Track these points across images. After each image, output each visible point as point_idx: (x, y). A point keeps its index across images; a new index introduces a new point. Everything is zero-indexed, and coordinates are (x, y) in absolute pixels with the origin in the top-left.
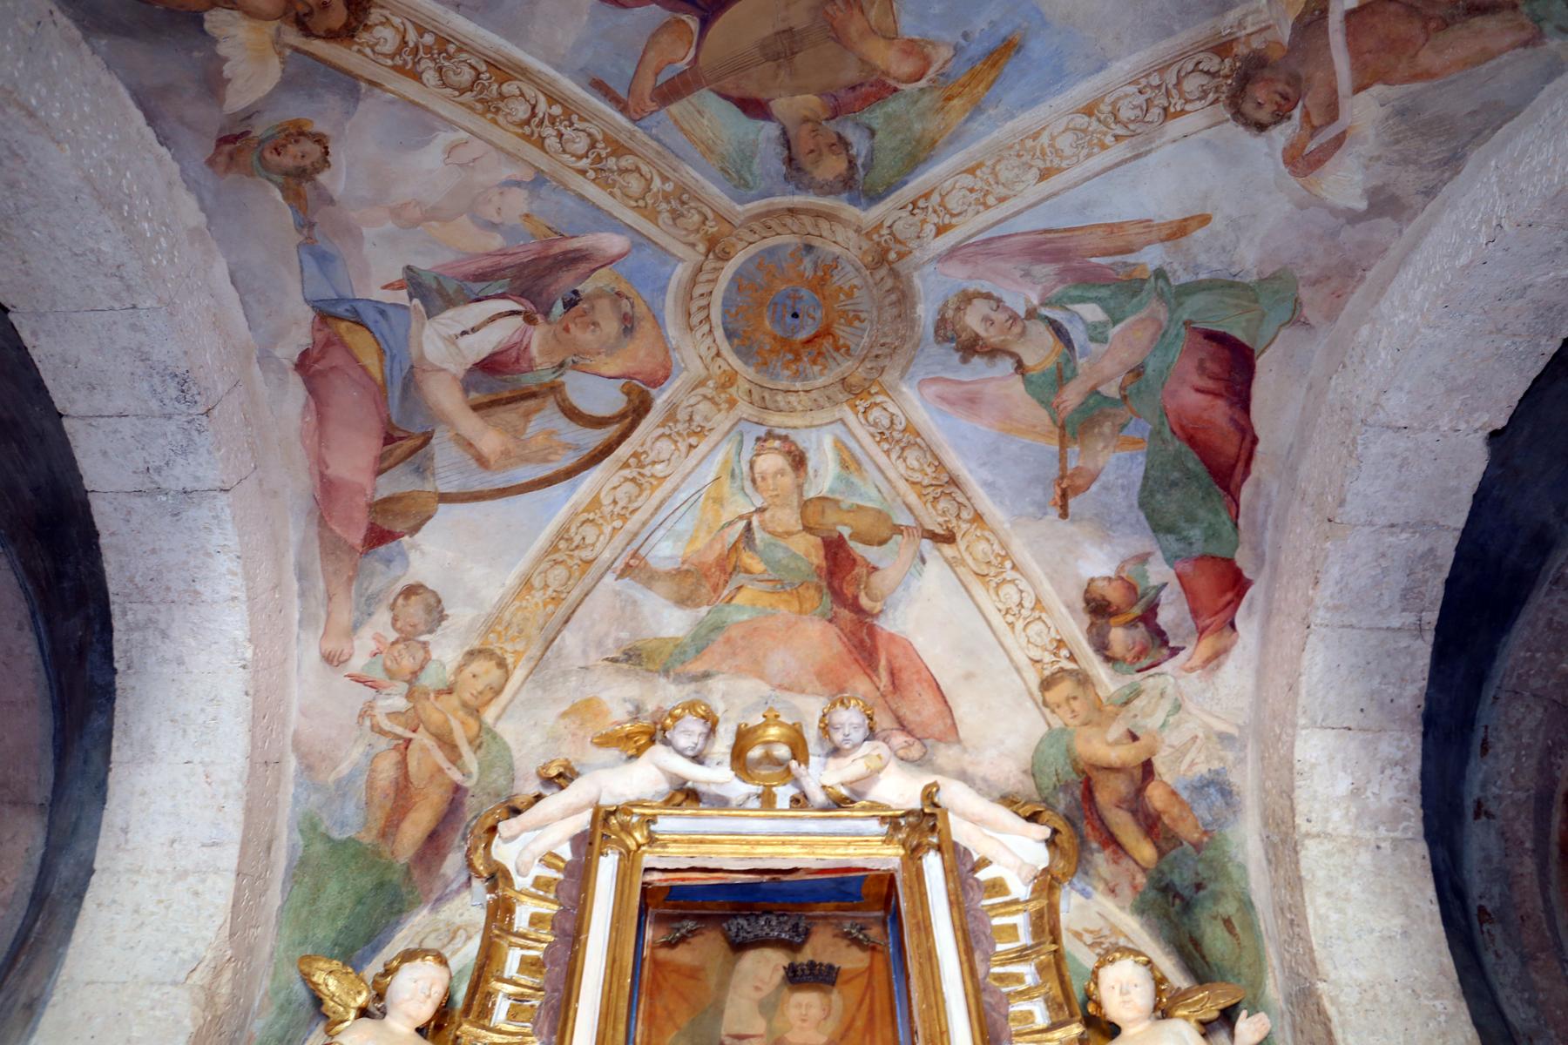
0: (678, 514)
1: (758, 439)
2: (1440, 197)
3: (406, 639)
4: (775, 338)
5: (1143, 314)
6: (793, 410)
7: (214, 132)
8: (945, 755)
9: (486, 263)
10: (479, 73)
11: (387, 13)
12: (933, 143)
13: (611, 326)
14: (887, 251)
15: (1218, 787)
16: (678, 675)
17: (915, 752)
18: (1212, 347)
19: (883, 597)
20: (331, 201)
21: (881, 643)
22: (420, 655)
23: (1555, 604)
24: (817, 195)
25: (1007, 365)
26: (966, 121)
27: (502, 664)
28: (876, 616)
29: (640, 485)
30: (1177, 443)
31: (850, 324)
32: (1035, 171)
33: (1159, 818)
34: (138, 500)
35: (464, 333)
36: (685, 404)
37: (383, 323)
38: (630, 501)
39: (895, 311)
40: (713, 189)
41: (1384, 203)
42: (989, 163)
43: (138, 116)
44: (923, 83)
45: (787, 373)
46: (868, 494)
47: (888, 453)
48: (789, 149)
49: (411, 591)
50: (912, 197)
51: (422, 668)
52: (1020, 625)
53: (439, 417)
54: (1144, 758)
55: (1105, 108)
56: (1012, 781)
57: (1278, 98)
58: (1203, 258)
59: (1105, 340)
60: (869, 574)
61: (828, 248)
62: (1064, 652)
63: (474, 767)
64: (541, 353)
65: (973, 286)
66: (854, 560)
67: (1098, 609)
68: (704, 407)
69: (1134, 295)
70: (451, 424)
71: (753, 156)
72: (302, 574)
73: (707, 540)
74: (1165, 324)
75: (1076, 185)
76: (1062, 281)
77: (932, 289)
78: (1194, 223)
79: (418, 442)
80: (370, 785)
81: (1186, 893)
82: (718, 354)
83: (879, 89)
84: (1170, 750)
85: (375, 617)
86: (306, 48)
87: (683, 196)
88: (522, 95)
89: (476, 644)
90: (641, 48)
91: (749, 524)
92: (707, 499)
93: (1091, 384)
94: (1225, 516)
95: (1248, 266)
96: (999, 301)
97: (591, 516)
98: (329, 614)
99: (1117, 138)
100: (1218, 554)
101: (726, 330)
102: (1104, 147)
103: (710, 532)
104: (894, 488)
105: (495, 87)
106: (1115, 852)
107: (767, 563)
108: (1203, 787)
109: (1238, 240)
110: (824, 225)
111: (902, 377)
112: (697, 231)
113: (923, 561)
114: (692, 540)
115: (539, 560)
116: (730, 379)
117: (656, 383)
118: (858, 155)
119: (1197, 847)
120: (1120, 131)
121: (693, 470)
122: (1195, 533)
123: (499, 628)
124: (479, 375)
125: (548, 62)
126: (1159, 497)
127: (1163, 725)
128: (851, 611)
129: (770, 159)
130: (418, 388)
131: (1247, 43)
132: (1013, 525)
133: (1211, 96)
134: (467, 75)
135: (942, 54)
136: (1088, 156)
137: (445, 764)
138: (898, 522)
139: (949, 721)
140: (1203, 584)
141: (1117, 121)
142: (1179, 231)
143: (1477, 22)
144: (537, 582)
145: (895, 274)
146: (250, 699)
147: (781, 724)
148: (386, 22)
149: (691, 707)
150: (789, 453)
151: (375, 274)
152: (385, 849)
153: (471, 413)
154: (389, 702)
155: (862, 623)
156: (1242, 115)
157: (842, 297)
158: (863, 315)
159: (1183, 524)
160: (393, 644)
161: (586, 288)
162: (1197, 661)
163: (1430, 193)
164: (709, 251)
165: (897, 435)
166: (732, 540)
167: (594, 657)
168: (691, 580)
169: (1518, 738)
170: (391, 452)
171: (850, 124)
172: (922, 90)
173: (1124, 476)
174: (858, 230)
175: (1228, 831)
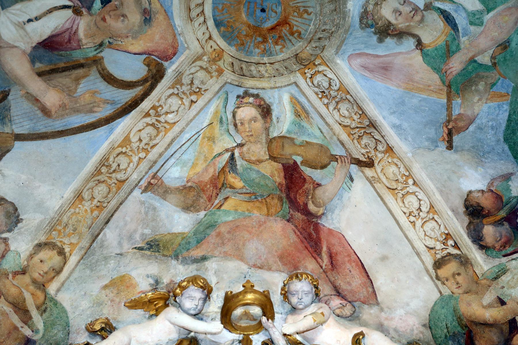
0: (184, 148)
1: (238, 97)
4: (249, 26)
6: (262, 77)
8: (369, 313)
16: (184, 258)
17: (348, 311)
19: (324, 204)
25: (410, 43)
27: (61, 252)
28: (320, 217)
29: (157, 129)
31: (301, 16)
35: (30, 21)
36: (188, 72)
38: (151, 140)
45: (257, 51)
46: (313, 134)
47: (327, 105)
52: (419, 223)
54: (510, 318)
56: (416, 332)
59: (481, 24)
60: (315, 188)
62: (450, 242)
63: (40, 326)
64: (86, 36)
67: (474, 212)
68: (201, 75)
73: (204, 165)
82: (210, 38)
89: (43, 239)
91: (233, 155)
92: (203, 138)
93: (471, 55)
97: (124, 150)
101: (215, 20)
103: (205, 161)
104: (332, 129)
107: (245, 181)
111: (337, 53)
113: (352, 180)
114: (194, 165)
116: (219, 54)
117: (168, 58)
121: (194, 117)
123: (59, 228)
124: (41, 51)
132: (414, 154)
137: (19, 324)
138: (334, 153)
144: (86, 195)
147: (256, 292)
149: (193, 280)
150: (260, 106)
153: (37, 78)
155: (310, 222)
158: (310, 10)
165: (333, 93)
166: (221, 166)
167: (127, 247)
173: (493, 120)
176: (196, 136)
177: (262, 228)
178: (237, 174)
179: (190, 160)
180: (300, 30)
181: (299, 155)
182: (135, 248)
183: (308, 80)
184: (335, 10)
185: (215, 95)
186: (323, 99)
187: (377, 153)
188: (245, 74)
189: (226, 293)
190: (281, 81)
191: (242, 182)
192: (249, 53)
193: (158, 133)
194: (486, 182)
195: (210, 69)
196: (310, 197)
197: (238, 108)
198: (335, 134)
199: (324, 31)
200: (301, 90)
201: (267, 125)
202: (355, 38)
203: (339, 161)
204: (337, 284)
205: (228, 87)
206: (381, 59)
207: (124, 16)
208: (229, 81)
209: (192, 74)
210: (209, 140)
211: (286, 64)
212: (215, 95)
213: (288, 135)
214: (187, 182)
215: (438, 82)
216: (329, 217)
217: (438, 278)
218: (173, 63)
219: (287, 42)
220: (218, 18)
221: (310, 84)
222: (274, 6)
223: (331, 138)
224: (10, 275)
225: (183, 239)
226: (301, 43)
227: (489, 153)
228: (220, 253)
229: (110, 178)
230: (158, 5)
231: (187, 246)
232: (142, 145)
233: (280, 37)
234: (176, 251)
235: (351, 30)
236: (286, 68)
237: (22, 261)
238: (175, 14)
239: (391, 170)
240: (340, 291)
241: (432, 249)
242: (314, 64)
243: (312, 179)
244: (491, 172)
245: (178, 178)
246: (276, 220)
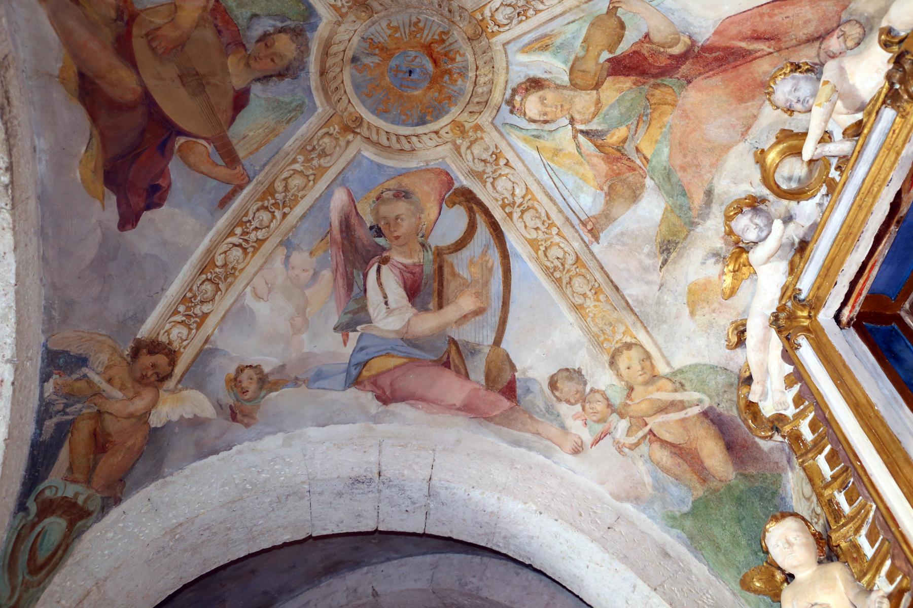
0: (559, 185)
1: (512, 112)
3: (584, 401)
4: (429, 88)
6: (492, 81)
7: (227, 423)
9: (340, 282)
10: (207, 280)
11: (162, 332)
13: (401, 207)
19: (677, 34)
20: (283, 367)
21: (722, 43)
22: (598, 396)
24: (308, 56)
27: (629, 346)
28: (693, 43)
29: (529, 208)
31: (423, 30)
34: (432, 516)
35: (386, 303)
36: (471, 164)
37: (367, 350)
38: (539, 218)
40: (303, 128)
43: (213, 459)
45: (460, 82)
46: (575, 32)
47: (537, 11)
48: (271, 76)
49: (553, 384)
51: (607, 399)
53: (441, 332)
60: (650, 42)
63: (696, 396)
64: (411, 257)
66: (634, 52)
68: (477, 149)
70: (448, 324)
72: (517, 443)
73: (587, 167)
79: (454, 348)
80: (667, 471)
82: (437, 133)
85: (561, 412)
86: (179, 377)
87: (308, 149)
88: (225, 252)
89: (606, 358)
90: (198, 175)
91: (582, 132)
92: (553, 161)
97: (542, 248)
98: (549, 439)
101: (418, 125)
103: (581, 164)
104: (571, 9)
105: (217, 270)
107: (621, 124)
110: (334, 49)
112: (337, 139)
114: (584, 178)
115: (564, 294)
116: (458, 126)
117: (450, 182)
118: (274, 26)
121: (526, 166)
123: (602, 338)
124: (418, 300)
125: (205, 235)
128: (684, 63)
129: (281, 89)
130: (418, 338)
134: (208, 287)
137: (682, 415)
138: (605, 10)
144: (579, 300)
146: (560, 521)
148: (168, 332)
150: (527, 90)
151: (337, 349)
152: (714, 484)
153: (443, 311)
154: (620, 430)
155: (698, 56)
157: (398, 35)
158: (414, 19)
160: (584, 409)
161: (369, 220)
164: (354, 132)
167: (655, 277)
168: (618, 187)
170: (456, 366)
171: (248, 33)
174: (339, 24)
176: (548, 168)
177: (691, 115)
178: (608, 131)
179: (575, 182)
180: (438, 31)
181: (599, 55)
183: (501, 29)
185: (504, 138)
186: (528, 15)
188: (485, 99)
190: (500, 62)
191: (620, 128)
192: (461, 92)
195: (472, 139)
196: (662, 50)
197: (525, 114)
198: (578, 6)
199: (440, 6)
200: (514, 39)
201: (552, 85)
203: (617, 5)
204: (804, 37)
205: (498, 122)
207: (397, 218)
208: (490, 120)
209: (474, 159)
210: (556, 155)
211: (479, 52)
212: (504, 138)
213: (570, 64)
214: (602, 189)
218: (457, 177)
219: (452, 47)
220: (416, 121)
221: (507, 28)
222: (408, 59)
223: (583, 11)
224: (629, 402)
225: (672, 211)
226: (455, 33)
228: (710, 172)
229: (568, 271)
230: (393, 182)
231: (684, 208)
232: (543, 228)
236: (484, 52)
237: (620, 386)
238: (403, 166)
240: (816, 35)
242: (481, 21)
243: (636, 43)
245: (594, 199)
246: (684, 97)
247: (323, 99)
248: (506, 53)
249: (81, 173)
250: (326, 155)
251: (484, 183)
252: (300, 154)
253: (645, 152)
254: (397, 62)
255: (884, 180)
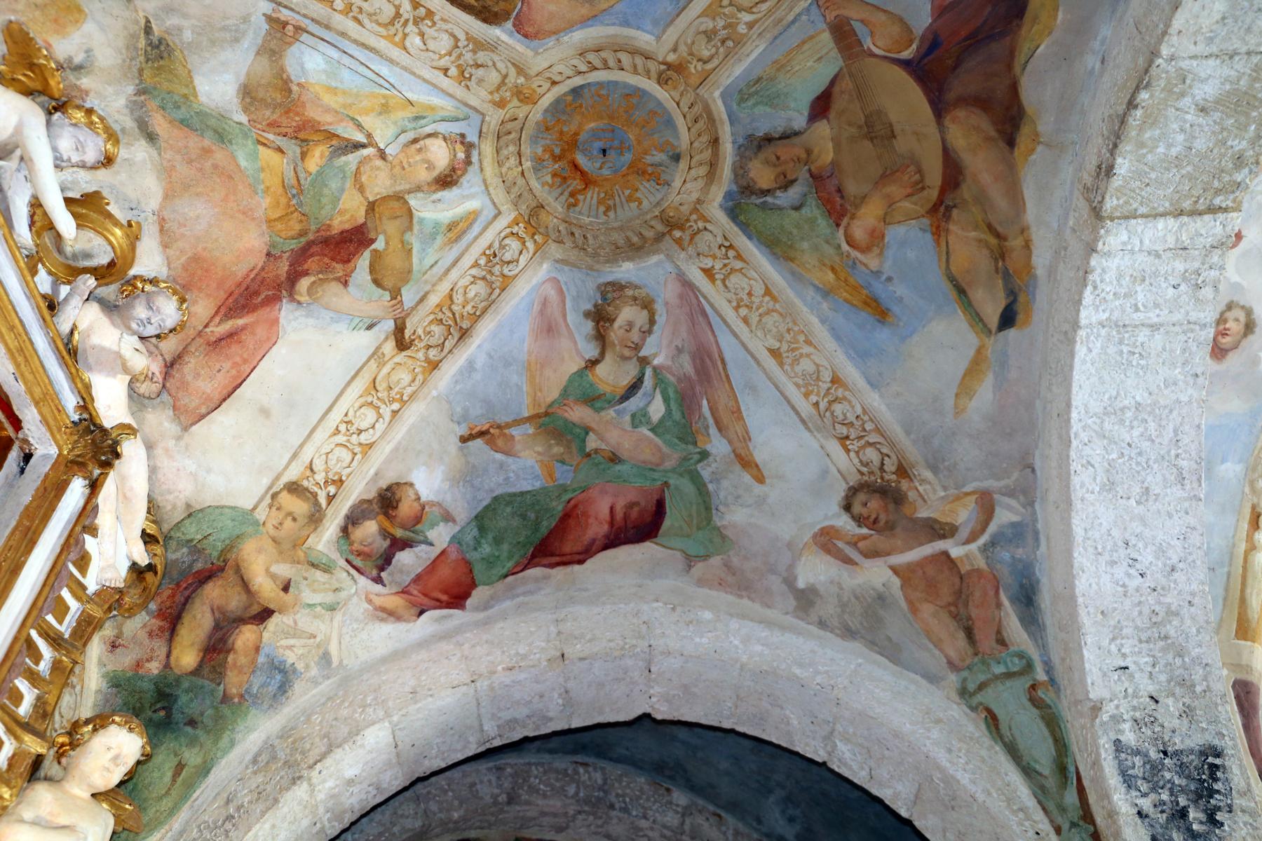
0: (362, 69)
1: (463, 136)
2: (822, 633)
4: (576, 134)
5: (665, 449)
6: (500, 164)
8: (159, 421)
12: (792, 260)
14: (681, 228)
15: (284, 677)
16: (143, 105)
18: (651, 507)
19: (316, 300)
21: (263, 313)
23: (486, 779)
25: (591, 351)
26: (815, 286)
28: (292, 298)
29: (392, 23)
30: (560, 508)
31: (600, 202)
32: (777, 345)
33: (229, 651)
36: (496, 58)
38: (370, 15)
39: (621, 242)
40: (738, 70)
41: (806, 600)
42: (777, 306)
44: (845, 247)
45: (540, 151)
46: (425, 257)
47: (476, 265)
48: (780, 138)
50: (736, 244)
52: (341, 439)
54: (272, 606)
55: (840, 393)
56: (171, 497)
57: (873, 516)
58: (725, 483)
59: (635, 426)
60: (338, 279)
61: (678, 176)
62: (332, 490)
65: (659, 307)
66: (349, 261)
67: (387, 501)
68: (494, 78)
69: (680, 439)
71: (773, 106)
73: (334, 105)
74: (662, 468)
75: (770, 379)
76: (679, 380)
77: (649, 272)
78: (755, 471)
81: (177, 716)
82: (554, 83)
83: (838, 209)
84: (291, 623)
87: (731, 42)
90: (890, 9)
91: (364, 146)
92: (384, 97)
93: (593, 425)
94: (510, 565)
95: (728, 517)
96: (650, 332)
99: (816, 404)
100: (476, 572)
101: (582, 87)
102: (806, 395)
103: (344, 106)
104: (440, 279)
106: (161, 629)
107: (320, 173)
108: (276, 668)
109: (749, 506)
110: (703, 171)
111: (557, 261)
112: (691, 54)
113: (369, 327)
114: (333, 91)
116: (526, 98)
117: (519, 27)
118: (776, 198)
119: (226, 698)
120: (823, 405)
121: (419, 77)
122: (486, 549)
126: (509, 510)
127: (309, 605)
129: (768, 121)
131: (910, 488)
132: (438, 398)
133: (865, 470)
135: (872, 262)
136: (798, 386)
138: (404, 291)
139: (203, 410)
140: (445, 572)
141: (830, 403)
142: (746, 462)
143: (961, 635)
145: (659, 238)
150: (454, 170)
156: (854, 494)
158: (611, 214)
159: (490, 536)
162: (378, 601)
163: (822, 624)
165: (497, 270)
166: (340, 131)
168: (279, 97)
169: (393, 824)
171: (805, 189)
172: (839, 246)
174: (699, 201)
175: (253, 711)
176: (387, 85)
177: (241, 216)
179: (342, 82)
181: (387, 243)
182: (148, 21)
183: (508, 230)
184: (618, 248)
187: (423, 351)
189: (97, 193)
190: (500, 195)
192: (534, 140)
193: (385, 26)
194: (432, 497)
195: (504, 88)
197: (445, 139)
198: (434, 285)
200: (490, 223)
202: (583, 281)
204: (187, 359)
206: (561, 320)
209: (494, 65)
210: (383, 105)
211: (525, 194)
213: (415, 220)
214: (299, 84)
215: (549, 400)
216: (297, 313)
217: (274, 496)
219: (560, 190)
220: (586, 90)
221: (503, 235)
223: (426, 282)
225: (185, 96)
227: (472, 486)
231: (170, 105)
233: (565, 179)
234: (155, 88)
235: (595, 274)
236: (520, 196)
238: (591, 29)
239: (403, 376)
241: (312, 470)
242: (534, 234)
243: (352, 271)
244: (449, 497)
245: (302, 68)
247: (713, 108)
248: (494, 204)
249: (1055, 19)
250: (705, 32)
251: (469, 38)
252: (745, 35)
253: (269, 152)
254: (622, 159)
255: (22, 375)
